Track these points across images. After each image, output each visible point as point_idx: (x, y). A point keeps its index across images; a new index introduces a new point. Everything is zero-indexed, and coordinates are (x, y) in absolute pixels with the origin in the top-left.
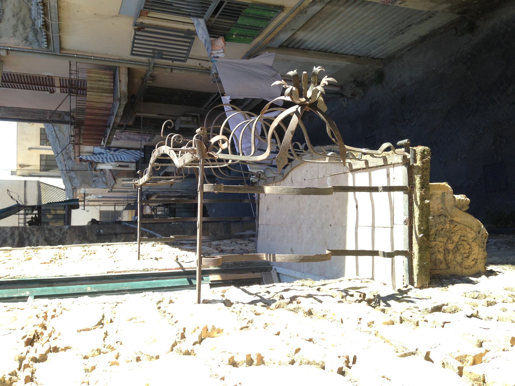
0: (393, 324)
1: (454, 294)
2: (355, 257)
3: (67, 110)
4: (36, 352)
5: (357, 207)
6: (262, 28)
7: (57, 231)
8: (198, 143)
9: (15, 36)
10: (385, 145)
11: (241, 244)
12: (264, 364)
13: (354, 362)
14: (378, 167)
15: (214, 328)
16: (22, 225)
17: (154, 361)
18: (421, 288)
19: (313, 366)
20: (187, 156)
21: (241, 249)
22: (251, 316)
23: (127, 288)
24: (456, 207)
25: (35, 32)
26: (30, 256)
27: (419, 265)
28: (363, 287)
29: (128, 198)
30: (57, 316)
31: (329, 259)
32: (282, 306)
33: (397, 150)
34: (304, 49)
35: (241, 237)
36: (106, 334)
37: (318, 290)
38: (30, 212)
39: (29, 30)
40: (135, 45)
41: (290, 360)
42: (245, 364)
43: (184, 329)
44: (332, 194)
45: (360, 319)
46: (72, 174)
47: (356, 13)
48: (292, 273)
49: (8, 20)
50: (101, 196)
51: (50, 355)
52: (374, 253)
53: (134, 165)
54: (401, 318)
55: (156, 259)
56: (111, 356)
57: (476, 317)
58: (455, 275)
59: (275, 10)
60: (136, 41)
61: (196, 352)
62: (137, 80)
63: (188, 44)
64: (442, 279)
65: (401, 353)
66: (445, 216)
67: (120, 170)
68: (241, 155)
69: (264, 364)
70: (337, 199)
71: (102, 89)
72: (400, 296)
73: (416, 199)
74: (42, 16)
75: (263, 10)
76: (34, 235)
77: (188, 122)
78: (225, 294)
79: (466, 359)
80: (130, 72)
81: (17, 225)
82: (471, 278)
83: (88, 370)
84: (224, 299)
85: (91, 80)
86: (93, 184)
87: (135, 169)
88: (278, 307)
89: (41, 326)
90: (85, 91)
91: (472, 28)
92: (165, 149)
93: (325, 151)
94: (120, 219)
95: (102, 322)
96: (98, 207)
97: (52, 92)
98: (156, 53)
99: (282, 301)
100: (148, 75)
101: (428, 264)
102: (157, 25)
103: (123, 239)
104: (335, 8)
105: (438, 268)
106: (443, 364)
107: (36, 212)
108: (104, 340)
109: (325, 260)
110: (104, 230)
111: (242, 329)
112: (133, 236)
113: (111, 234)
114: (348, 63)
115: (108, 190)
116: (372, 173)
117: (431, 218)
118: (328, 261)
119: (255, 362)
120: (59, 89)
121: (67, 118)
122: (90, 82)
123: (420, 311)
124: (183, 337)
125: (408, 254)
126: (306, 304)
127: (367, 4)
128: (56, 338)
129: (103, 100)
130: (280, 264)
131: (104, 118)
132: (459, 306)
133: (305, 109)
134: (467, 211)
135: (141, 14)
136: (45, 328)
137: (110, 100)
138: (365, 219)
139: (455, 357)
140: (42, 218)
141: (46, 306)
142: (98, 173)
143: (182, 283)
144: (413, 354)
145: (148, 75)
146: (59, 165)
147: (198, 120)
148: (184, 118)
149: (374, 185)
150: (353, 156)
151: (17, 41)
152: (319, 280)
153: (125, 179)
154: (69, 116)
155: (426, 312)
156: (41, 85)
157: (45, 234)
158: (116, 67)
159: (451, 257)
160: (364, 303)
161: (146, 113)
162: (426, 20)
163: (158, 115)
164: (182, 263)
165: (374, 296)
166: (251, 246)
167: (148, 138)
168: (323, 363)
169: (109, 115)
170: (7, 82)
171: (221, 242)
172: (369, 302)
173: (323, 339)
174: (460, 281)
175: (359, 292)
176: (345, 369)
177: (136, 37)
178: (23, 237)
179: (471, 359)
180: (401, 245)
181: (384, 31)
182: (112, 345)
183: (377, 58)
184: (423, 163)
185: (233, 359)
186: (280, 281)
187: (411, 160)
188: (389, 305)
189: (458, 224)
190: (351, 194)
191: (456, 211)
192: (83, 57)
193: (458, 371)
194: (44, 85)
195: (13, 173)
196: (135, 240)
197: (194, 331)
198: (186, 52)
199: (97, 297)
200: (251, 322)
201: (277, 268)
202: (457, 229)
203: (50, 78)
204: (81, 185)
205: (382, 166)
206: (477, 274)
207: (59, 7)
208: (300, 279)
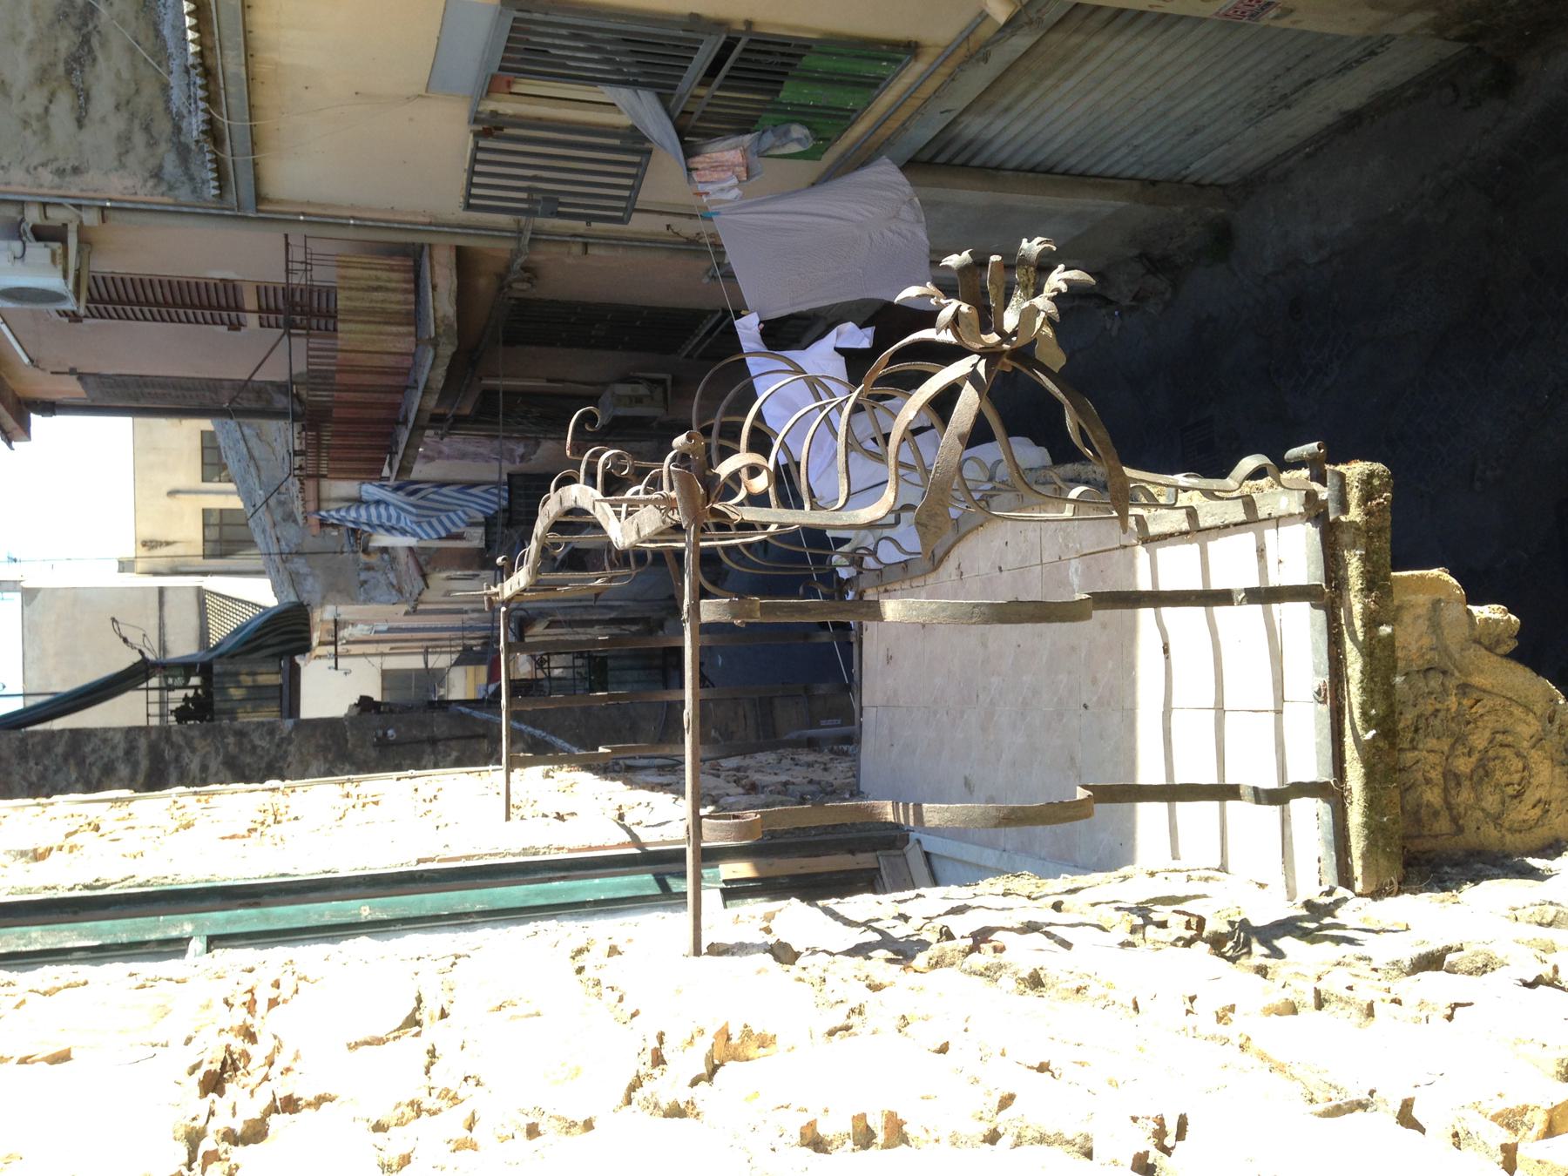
0: (1295, 1012)
1: (1479, 912)
2: (1165, 805)
3: (282, 376)
4: (234, 1114)
5: (1166, 650)
6: (854, 111)
7: (262, 738)
8: (680, 481)
9: (122, 166)
10: (1249, 463)
11: (810, 765)
12: (907, 1142)
13: (1180, 1135)
14: (1227, 526)
15: (747, 1033)
16: (155, 721)
17: (579, 1136)
18: (1377, 894)
19: (1056, 1148)
20: (646, 516)
21: (811, 782)
22: (858, 994)
23: (478, 907)
24: (1477, 641)
25: (183, 152)
26: (188, 818)
27: (1366, 825)
28: (1196, 897)
29: (463, 629)
30: (285, 1001)
31: (1088, 816)
32: (947, 961)
33: (1285, 476)
34: (982, 167)
35: (812, 744)
36: (432, 1053)
37: (1057, 907)
38: (179, 681)
39: (163, 147)
40: (476, 180)
41: (984, 1128)
42: (850, 1144)
43: (661, 1037)
44: (1090, 617)
45: (1192, 999)
46: (299, 564)
47: (1140, 51)
48: (970, 852)
49: (103, 120)
50: (385, 628)
51: (274, 1120)
52: (1225, 792)
53: (480, 531)
54: (1317, 992)
55: (560, 817)
56: (452, 1122)
57: (1550, 984)
58: (1479, 853)
59: (891, 55)
60: (478, 168)
61: (700, 1107)
62: (483, 283)
63: (633, 171)
64: (1442, 865)
65: (1322, 1106)
66: (1444, 673)
67: (439, 549)
68: (807, 506)
69: (907, 1142)
70: (1104, 626)
71: (384, 311)
72: (1313, 924)
73: (1350, 624)
74: (202, 105)
75: (857, 57)
76: (193, 751)
77: (639, 400)
78: (772, 925)
79: (1526, 1119)
80: (464, 261)
81: (144, 723)
82: (1530, 860)
83: (390, 1166)
84: (771, 940)
85: (351, 289)
86: (360, 591)
87: (482, 545)
88: (937, 964)
89: (239, 1033)
90: (331, 321)
91: (1504, 82)
92: (581, 494)
93: (1060, 483)
94: (442, 692)
95: (418, 1017)
96: (377, 660)
97: (236, 326)
98: (537, 202)
99: (948, 945)
100: (516, 267)
101: (1395, 822)
102: (540, 119)
103: (454, 754)
104: (1076, 39)
105: (1426, 832)
106: (1456, 1135)
107: (195, 681)
108: (427, 1072)
109: (1076, 817)
110: (397, 731)
111: (831, 1033)
112: (485, 745)
113: (420, 742)
114: (1121, 204)
115: (405, 608)
116: (1211, 545)
117: (1398, 679)
118: (1082, 822)
119: (881, 1138)
120: (256, 316)
121: (282, 402)
122: (347, 293)
123: (1375, 970)
124: (658, 1060)
125: (1332, 793)
126: (1023, 953)
127: (1171, 26)
128: (288, 1070)
129: (390, 347)
130: (936, 831)
131: (388, 398)
132: (1499, 953)
133: (999, 367)
134: (1517, 656)
135: (492, 86)
136: (251, 1037)
137: (407, 345)
138: (1194, 687)
139: (1493, 1113)
140: (217, 698)
141: (251, 971)
142: (374, 560)
143: (638, 887)
144: (1363, 1106)
145: (516, 267)
146: (258, 538)
147: (665, 392)
148: (624, 389)
149: (1217, 584)
150: (1150, 496)
151: (129, 182)
152: (1056, 876)
153: (453, 573)
154: (286, 394)
155: (1395, 973)
156: (202, 307)
157: (226, 746)
158: (422, 246)
159: (1465, 796)
160: (1201, 948)
161: (515, 376)
162: (1359, 62)
163: (549, 381)
164: (635, 829)
165: (1231, 923)
166: (838, 773)
167: (520, 450)
168: (1087, 1138)
170: (102, 301)
171: (748, 761)
172: (1217, 942)
173: (1082, 1064)
174: (1496, 871)
175: (1184, 913)
176: (1155, 1156)
177: (480, 156)
178: (162, 756)
179: (1539, 1120)
180: (1309, 765)
181: (1230, 102)
182: (453, 1087)
183: (1211, 185)
184: (1369, 513)
185: (814, 1130)
186: (935, 882)
187: (1332, 507)
188: (1278, 954)
189: (1486, 697)
190: (1145, 615)
191: (1476, 654)
192: (322, 220)
193: (1500, 1158)
194: (210, 307)
195: (125, 566)
196: (491, 757)
197: (691, 1043)
198: (626, 193)
199: (394, 941)
200: (858, 1011)
201: (925, 839)
202: (1481, 711)
203: (230, 286)
204: (324, 598)
205: (1242, 523)
206: (1550, 846)
207: (250, 79)
208: (998, 872)
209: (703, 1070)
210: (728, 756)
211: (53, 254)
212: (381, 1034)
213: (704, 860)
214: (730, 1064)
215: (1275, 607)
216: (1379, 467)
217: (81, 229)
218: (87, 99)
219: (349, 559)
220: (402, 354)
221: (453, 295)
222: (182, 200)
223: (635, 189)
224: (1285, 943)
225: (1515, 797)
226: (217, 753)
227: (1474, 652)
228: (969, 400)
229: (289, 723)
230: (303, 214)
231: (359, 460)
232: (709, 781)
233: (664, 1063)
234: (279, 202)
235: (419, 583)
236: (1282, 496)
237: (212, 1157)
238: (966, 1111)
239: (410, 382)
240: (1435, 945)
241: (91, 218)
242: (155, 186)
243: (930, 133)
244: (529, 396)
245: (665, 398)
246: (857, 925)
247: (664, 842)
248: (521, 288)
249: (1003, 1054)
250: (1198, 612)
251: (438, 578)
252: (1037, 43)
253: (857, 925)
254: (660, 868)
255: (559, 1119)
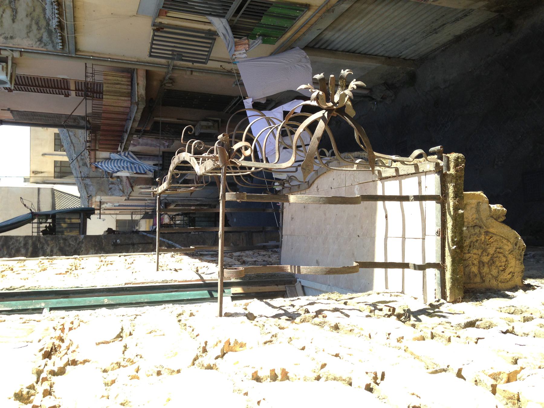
0: (424, 339)
1: (489, 309)
2: (384, 269)
3: (83, 114)
4: (54, 365)
5: (386, 217)
6: (287, 28)
7: (72, 241)
10: (417, 152)
11: (264, 255)
12: (289, 379)
13: (382, 379)
14: (409, 174)
15: (236, 342)
16: (35, 234)
18: (454, 302)
19: (340, 382)
20: (208, 163)
21: (264, 261)
23: (146, 300)
24: (492, 217)
26: (45, 267)
27: (451, 278)
28: (393, 301)
29: (145, 206)
30: (75, 329)
33: (429, 157)
34: (331, 50)
35: (264, 248)
36: (126, 347)
37: (345, 303)
38: (44, 221)
39: (43, 30)
40: (153, 46)
41: (316, 375)
42: (269, 379)
43: (206, 343)
45: (389, 334)
46: (88, 181)
47: (386, 11)
48: (317, 286)
49: (22, 20)
51: (68, 368)
52: (404, 265)
55: (176, 270)
56: (131, 370)
57: (511, 333)
60: (154, 42)
62: (155, 83)
63: (209, 45)
64: (477, 293)
65: (431, 370)
66: (480, 227)
67: (138, 178)
68: (265, 162)
69: (289, 379)
72: (432, 311)
73: (449, 209)
74: (57, 16)
76: (48, 245)
77: (209, 127)
79: (500, 377)
80: (149, 75)
82: (507, 292)
83: (108, 384)
84: (247, 312)
85: (108, 83)
86: (109, 191)
87: (153, 177)
88: (303, 321)
90: (101, 95)
91: (510, 27)
92: (186, 156)
93: (352, 158)
94: (137, 228)
95: (121, 335)
96: (114, 216)
97: (67, 95)
98: (175, 55)
99: (307, 315)
100: (167, 78)
101: (461, 277)
103: (140, 249)
104: (364, 6)
105: (472, 281)
106: (476, 381)
107: (50, 221)
108: (123, 353)
109: (353, 272)
110: (121, 240)
111: (265, 343)
112: (151, 246)
113: (129, 244)
114: (378, 65)
115: (125, 198)
116: (403, 181)
119: (280, 378)
121: (83, 123)
122: (107, 85)
123: (452, 326)
124: (205, 351)
125: (440, 267)
126: (333, 318)
128: (74, 351)
129: (120, 105)
130: (305, 277)
131: (121, 123)
132: (494, 321)
134: (504, 222)
135: (160, 13)
136: (62, 340)
137: (127, 104)
138: (395, 230)
140: (57, 227)
141: (63, 318)
142: (114, 180)
143: (202, 295)
144: (445, 370)
145: (167, 78)
146: (74, 172)
147: (219, 125)
148: (204, 123)
149: (404, 194)
151: (30, 42)
152: (346, 294)
153: (142, 186)
154: (84, 120)
155: (459, 328)
156: (55, 88)
157: (60, 244)
158: (134, 69)
159: (486, 270)
160: (394, 318)
162: (461, 18)
164: (202, 275)
165: (404, 310)
166: (274, 257)
167: (167, 144)
168: (350, 379)
169: (126, 120)
170: (20, 85)
171: (243, 254)
172: (399, 316)
173: (350, 355)
174: (495, 296)
175: (388, 306)
177: (155, 38)
179: (505, 377)
180: (433, 257)
181: (417, 31)
182: (132, 358)
183: (409, 59)
184: (457, 171)
185: (257, 374)
186: (305, 294)
187: (444, 168)
188: (419, 320)
190: (380, 203)
192: (99, 59)
193: (491, 389)
194: (58, 88)
195: (26, 180)
196: (154, 250)
198: (206, 53)
200: (275, 336)
201: (302, 281)
202: (492, 241)
203: (65, 81)
204: (96, 193)
205: (414, 174)
206: (514, 288)
207: (74, 7)
208: (326, 292)
209: (220, 354)
210: (236, 251)
211: (3, 67)
212: (108, 340)
213: (224, 286)
214: (230, 353)
215: (424, 202)
216: (461, 155)
217: (13, 58)
218: (16, 13)
219: (106, 182)
220: (126, 107)
221: (144, 87)
222: (49, 49)
223: (209, 52)
224: (422, 317)
225: (502, 271)
226: (57, 246)
227: (491, 220)
228: (321, 125)
229: (82, 236)
230: (92, 56)
231: (109, 144)
232: (228, 260)
233: (207, 352)
234: (83, 51)
235: (130, 189)
236: (428, 164)
237: (44, 379)
238: (309, 369)
239: (129, 118)
240: (473, 319)
241: (16, 55)
242: (40, 44)
243: (313, 37)
244: (171, 124)
245: (219, 127)
246: (277, 308)
247: (212, 280)
248: (169, 86)
249: (324, 351)
250: (398, 203)
251: (137, 188)
252: (351, 7)
253: (277, 308)
254: (210, 289)
255: (168, 369)
